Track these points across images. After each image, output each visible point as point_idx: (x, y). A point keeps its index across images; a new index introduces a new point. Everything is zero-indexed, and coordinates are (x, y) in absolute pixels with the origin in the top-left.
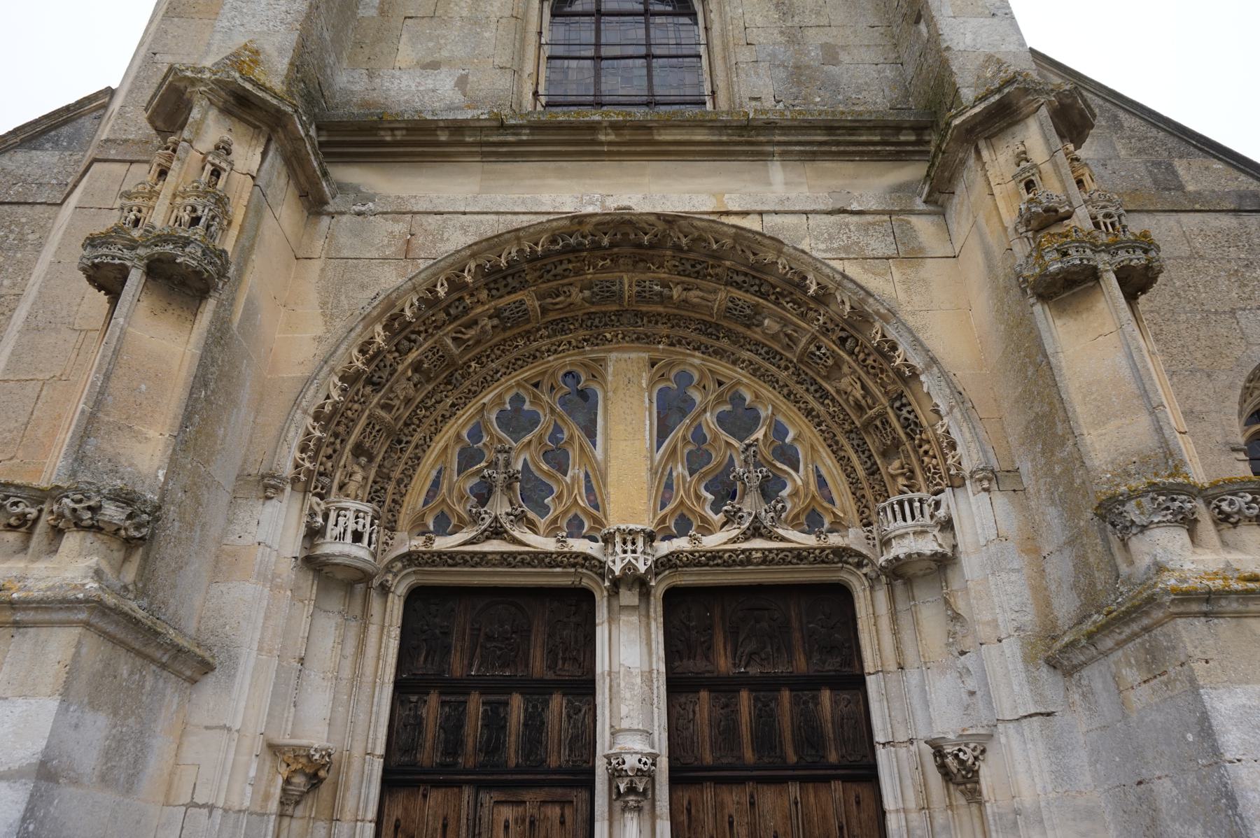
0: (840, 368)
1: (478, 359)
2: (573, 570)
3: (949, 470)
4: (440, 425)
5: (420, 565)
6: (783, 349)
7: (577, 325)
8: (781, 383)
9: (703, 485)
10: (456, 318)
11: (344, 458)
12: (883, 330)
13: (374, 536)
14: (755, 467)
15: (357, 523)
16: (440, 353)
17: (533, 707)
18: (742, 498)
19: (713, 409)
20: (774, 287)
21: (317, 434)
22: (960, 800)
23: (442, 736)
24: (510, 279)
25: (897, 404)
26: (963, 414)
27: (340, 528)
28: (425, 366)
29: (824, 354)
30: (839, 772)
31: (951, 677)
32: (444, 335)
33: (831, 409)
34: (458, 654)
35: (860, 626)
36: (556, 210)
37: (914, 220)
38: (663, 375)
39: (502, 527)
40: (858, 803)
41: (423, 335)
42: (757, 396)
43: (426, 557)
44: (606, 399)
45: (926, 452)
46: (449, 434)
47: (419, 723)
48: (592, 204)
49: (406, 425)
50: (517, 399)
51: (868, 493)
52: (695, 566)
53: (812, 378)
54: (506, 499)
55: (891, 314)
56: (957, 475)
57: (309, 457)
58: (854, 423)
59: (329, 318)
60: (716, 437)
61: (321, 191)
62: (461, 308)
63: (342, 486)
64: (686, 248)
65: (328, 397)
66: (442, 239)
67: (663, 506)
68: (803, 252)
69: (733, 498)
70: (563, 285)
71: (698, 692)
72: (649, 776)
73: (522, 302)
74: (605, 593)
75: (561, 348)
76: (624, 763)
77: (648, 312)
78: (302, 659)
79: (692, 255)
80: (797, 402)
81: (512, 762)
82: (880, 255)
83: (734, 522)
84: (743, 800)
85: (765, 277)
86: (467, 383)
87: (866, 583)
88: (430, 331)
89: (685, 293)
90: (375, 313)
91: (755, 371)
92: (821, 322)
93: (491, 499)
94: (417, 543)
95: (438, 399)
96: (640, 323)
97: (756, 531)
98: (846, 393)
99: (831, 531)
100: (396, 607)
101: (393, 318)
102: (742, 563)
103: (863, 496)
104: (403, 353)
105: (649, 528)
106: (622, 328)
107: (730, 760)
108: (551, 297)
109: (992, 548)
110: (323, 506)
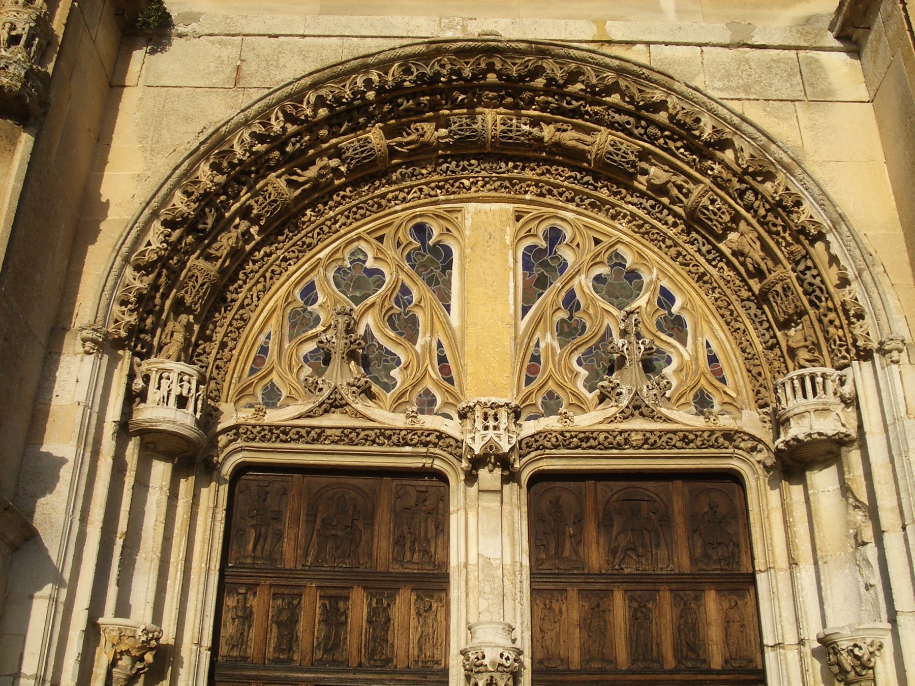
15: (181, 386)
17: (377, 603)
25: (801, 267)
30: (723, 677)
36: (410, 35)
38: (530, 231)
39: (342, 399)
43: (255, 431)
44: (463, 256)
66: (277, 66)
67: (529, 381)
68: (696, 89)
74: (462, 477)
75: (410, 197)
76: (484, 657)
89: (558, 133)
92: (716, 171)
97: (637, 408)
102: (619, 446)
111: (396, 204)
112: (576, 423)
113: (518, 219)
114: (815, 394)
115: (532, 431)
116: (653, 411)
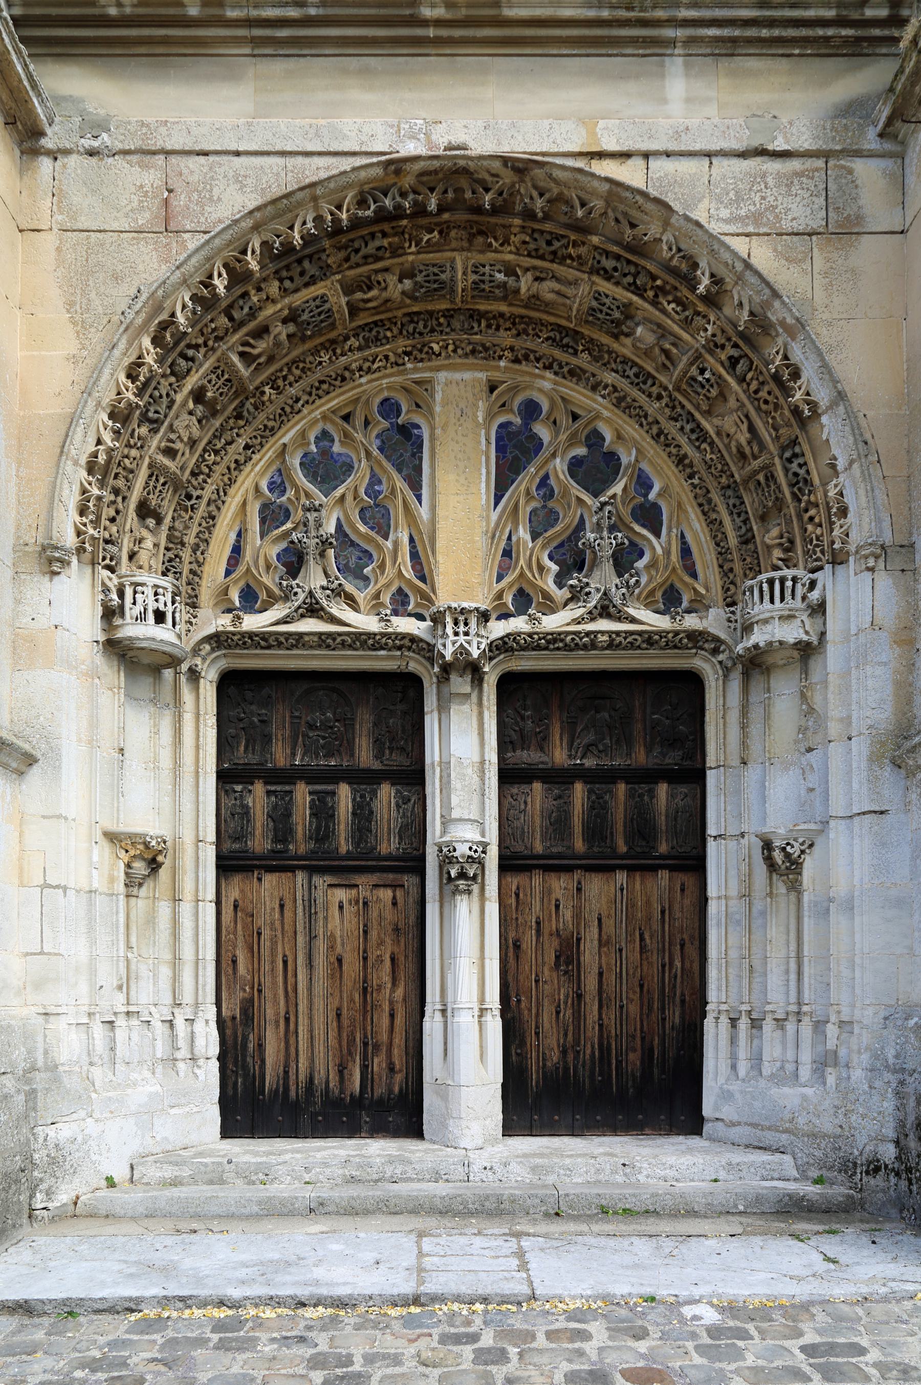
0: (725, 400)
1: (272, 382)
2: (399, 653)
3: (833, 543)
4: (235, 473)
5: (229, 647)
6: (657, 370)
7: (395, 331)
8: (650, 419)
9: (547, 552)
10: (242, 324)
11: (129, 521)
12: (786, 349)
13: (177, 615)
14: (610, 532)
15: (157, 600)
16: (226, 376)
17: (361, 797)
18: (591, 570)
19: (564, 453)
20: (654, 278)
21: (96, 491)
22: (781, 888)
23: (271, 824)
24: (306, 264)
25: (787, 454)
26: (862, 472)
27: (139, 608)
28: (209, 394)
29: (708, 380)
31: (794, 773)
32: (228, 349)
33: (708, 456)
34: (280, 743)
35: (707, 719)
37: (859, 166)
38: (503, 405)
39: (317, 603)
40: (682, 890)
41: (203, 350)
42: (619, 437)
43: (235, 638)
45: (811, 519)
46: (245, 485)
47: (246, 813)
48: (413, 137)
49: (194, 474)
50: (325, 435)
51: (738, 567)
52: (534, 649)
53: (689, 413)
54: (320, 570)
55: (797, 329)
56: (841, 549)
57: (91, 521)
58: (733, 476)
59: (81, 327)
60: (566, 492)
61: (31, 112)
62: (246, 310)
63: (132, 556)
64: (540, 215)
65: (99, 442)
66: (211, 199)
67: (500, 578)
68: (698, 224)
69: (580, 570)
70: (377, 272)
71: (531, 783)
72: (480, 863)
73: (323, 299)
74: (435, 680)
75: (376, 366)
76: (455, 850)
77: (487, 312)
78: (122, 749)
79: (548, 227)
80: (667, 445)
81: (343, 849)
82: (801, 229)
83: (579, 600)
84: (570, 887)
85: (642, 262)
86: (262, 416)
87: (720, 672)
88: (210, 343)
89: (536, 284)
90: (139, 321)
91: (621, 403)
92: (709, 333)
93: (303, 570)
94: (224, 622)
95: (229, 439)
96: (476, 329)
97: (605, 610)
98: (728, 435)
99: (689, 611)
100: (209, 694)
101: (164, 326)
102: (585, 647)
103: (731, 570)
104: (180, 377)
105: (483, 607)
106: (453, 336)
107: (560, 849)
108: (362, 290)
109: (862, 638)
110: (116, 581)
111: (361, 376)
112: (544, 624)
113: (492, 389)
114: (782, 599)
115: (501, 634)
116: (620, 611)
